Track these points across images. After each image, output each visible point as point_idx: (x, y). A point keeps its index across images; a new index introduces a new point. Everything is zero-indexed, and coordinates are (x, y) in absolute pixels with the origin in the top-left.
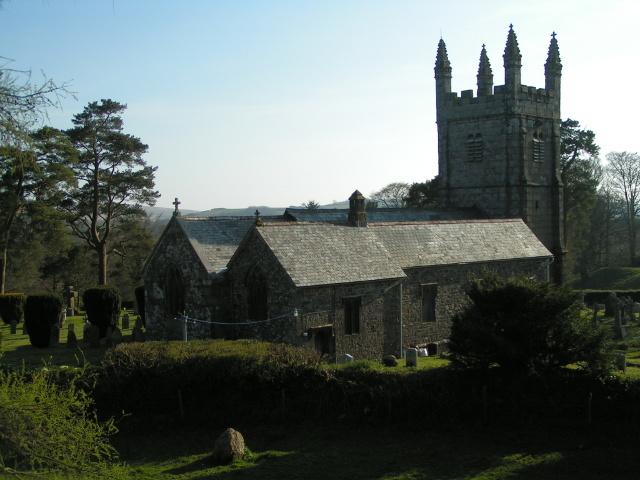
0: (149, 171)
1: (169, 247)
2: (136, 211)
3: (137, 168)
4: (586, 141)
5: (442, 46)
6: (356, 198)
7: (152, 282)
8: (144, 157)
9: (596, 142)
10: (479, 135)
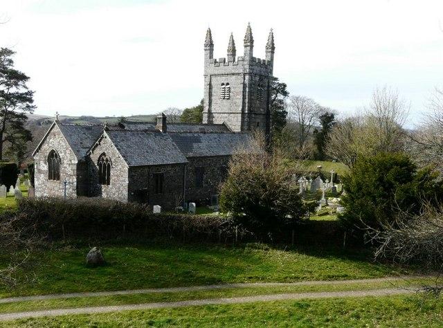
0: (30, 93)
1: (51, 140)
2: (23, 116)
3: (22, 90)
4: (282, 89)
5: (209, 32)
8: (27, 83)
9: (287, 89)
10: (228, 84)
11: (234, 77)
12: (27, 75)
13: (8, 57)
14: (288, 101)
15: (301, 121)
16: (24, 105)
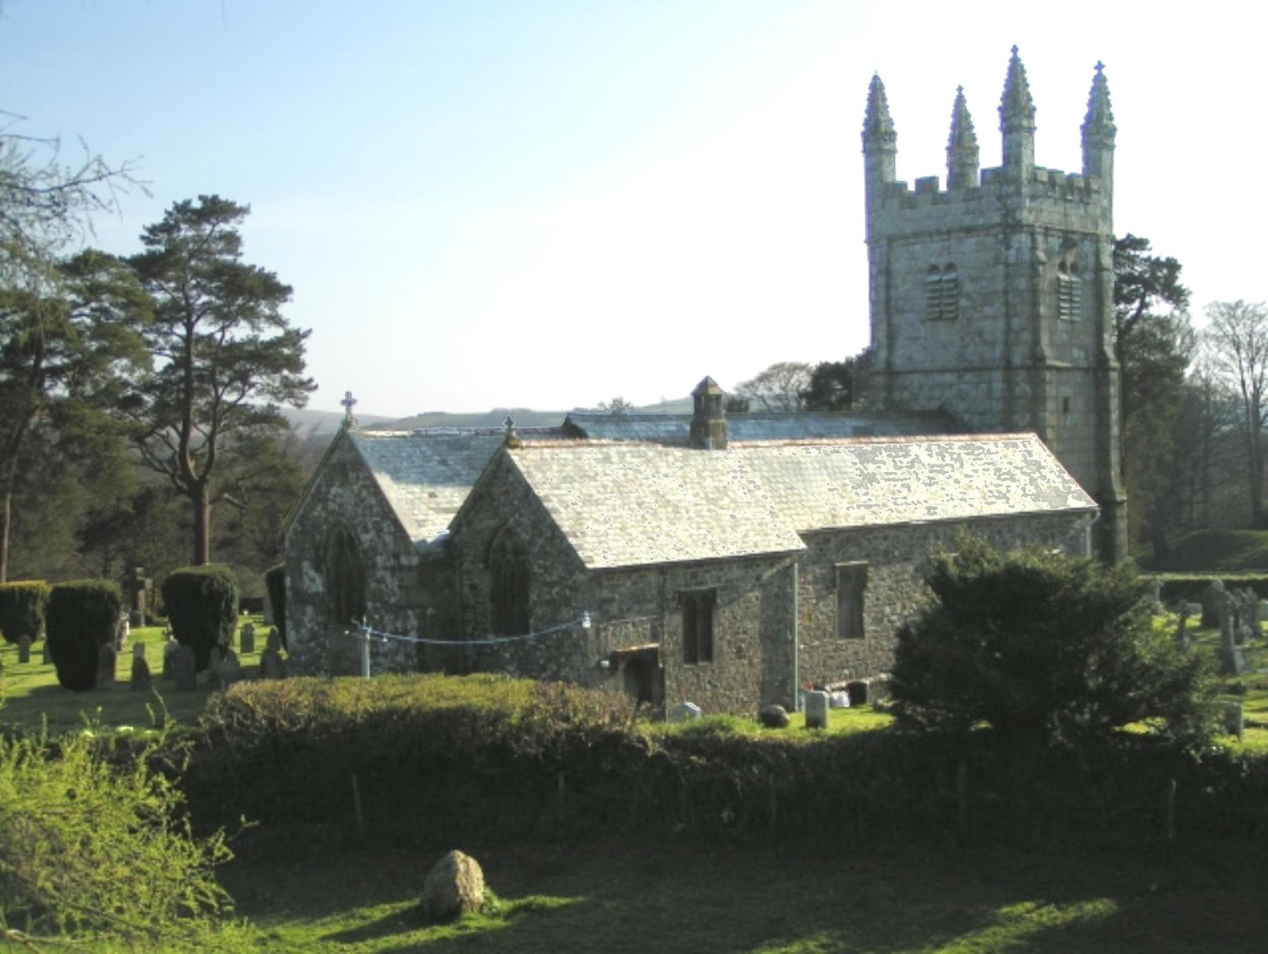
1: (333, 491)
2: (268, 417)
3: (269, 333)
6: (705, 396)
7: (299, 559)
8: (284, 310)
11: (971, 242)
12: (283, 280)
13: (226, 227)
14: (1198, 317)
15: (1250, 389)
16: (276, 380)
